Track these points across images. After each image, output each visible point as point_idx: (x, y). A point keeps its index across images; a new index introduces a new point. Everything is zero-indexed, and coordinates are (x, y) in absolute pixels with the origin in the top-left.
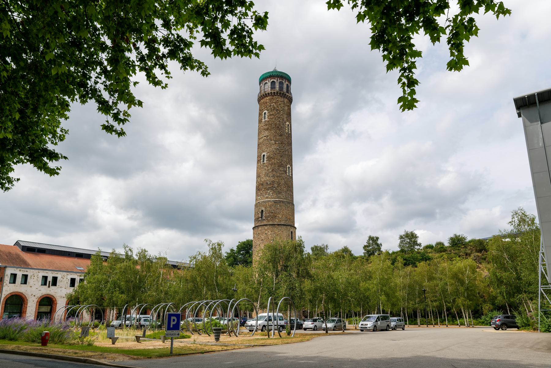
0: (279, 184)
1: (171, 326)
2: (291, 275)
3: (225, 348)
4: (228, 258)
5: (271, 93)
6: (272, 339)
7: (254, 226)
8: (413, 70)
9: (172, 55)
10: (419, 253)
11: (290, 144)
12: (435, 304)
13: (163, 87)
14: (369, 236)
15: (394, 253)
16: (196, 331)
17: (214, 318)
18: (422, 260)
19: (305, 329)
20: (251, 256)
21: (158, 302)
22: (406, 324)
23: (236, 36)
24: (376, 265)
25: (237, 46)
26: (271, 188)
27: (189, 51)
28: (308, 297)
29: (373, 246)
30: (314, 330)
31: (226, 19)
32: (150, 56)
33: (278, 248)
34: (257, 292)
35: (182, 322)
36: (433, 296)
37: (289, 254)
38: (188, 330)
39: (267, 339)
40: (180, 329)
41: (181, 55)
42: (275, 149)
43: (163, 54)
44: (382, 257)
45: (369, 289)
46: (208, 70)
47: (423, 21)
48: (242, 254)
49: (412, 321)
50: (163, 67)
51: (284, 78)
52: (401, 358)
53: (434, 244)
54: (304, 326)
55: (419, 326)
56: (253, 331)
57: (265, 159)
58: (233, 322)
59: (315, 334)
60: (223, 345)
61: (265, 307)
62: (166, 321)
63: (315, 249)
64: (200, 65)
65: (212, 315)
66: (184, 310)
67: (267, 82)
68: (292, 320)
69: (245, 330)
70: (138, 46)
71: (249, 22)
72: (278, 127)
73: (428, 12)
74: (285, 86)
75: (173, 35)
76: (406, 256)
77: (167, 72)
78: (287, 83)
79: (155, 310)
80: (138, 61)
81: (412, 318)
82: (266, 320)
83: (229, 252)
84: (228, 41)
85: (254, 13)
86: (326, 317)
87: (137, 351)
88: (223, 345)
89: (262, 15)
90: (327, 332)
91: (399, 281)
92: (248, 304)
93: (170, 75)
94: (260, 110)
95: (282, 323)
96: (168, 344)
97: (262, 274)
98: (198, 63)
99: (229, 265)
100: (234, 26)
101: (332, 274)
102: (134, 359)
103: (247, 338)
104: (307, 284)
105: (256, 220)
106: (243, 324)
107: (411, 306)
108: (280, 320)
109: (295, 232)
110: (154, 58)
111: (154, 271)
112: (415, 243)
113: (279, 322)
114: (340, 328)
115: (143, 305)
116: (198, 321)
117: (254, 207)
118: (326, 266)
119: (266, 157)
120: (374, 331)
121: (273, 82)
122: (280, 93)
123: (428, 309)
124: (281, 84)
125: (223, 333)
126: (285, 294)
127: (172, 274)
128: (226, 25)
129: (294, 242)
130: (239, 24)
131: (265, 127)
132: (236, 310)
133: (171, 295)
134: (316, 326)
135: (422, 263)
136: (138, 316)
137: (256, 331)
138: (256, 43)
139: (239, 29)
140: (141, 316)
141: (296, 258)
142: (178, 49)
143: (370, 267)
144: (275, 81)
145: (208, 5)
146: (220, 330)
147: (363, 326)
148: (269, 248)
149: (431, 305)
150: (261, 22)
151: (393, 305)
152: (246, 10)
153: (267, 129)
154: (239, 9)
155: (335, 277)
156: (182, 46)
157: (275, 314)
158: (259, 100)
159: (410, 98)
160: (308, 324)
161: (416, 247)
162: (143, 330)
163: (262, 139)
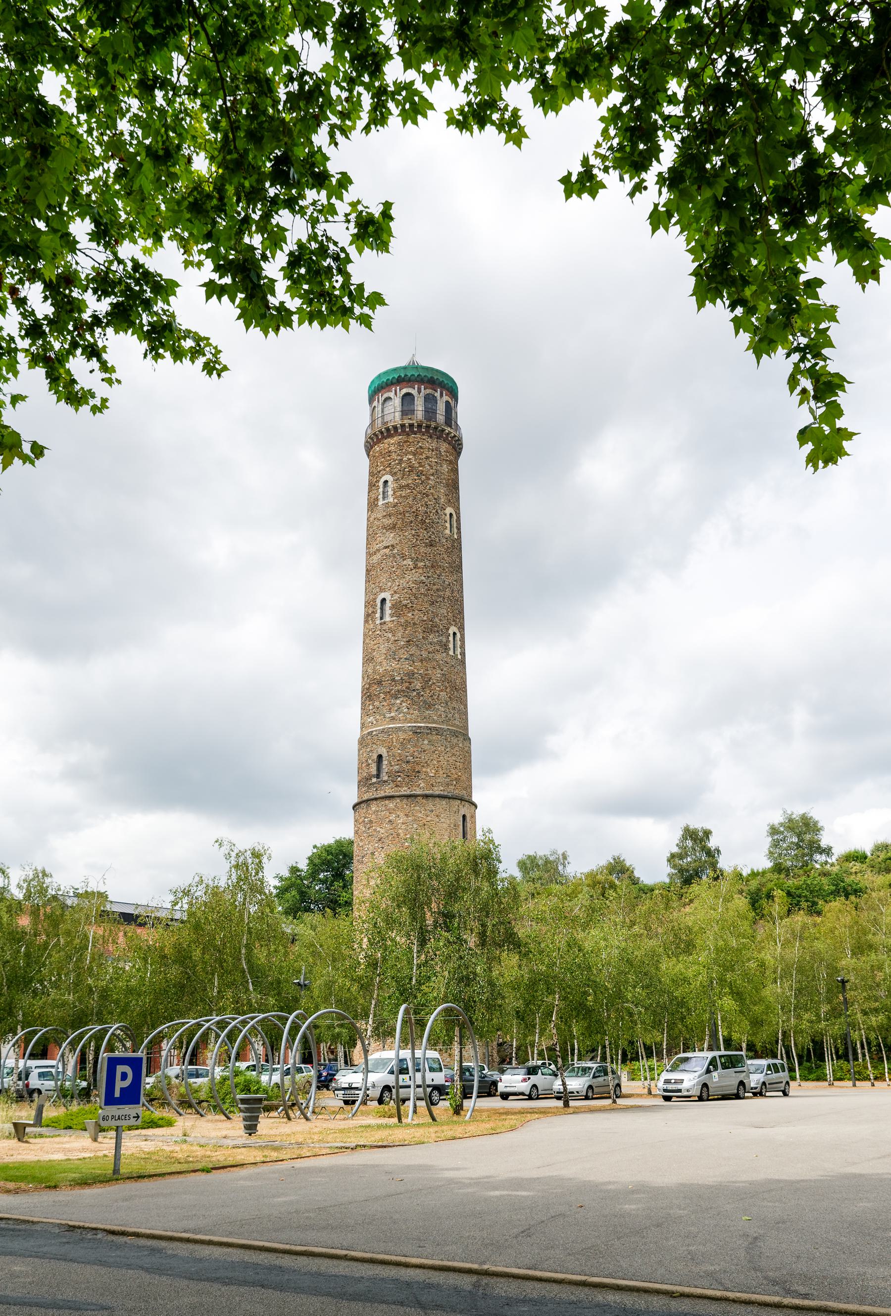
0: (427, 681)
1: (117, 1094)
2: (460, 941)
3: (274, 1155)
4: (282, 892)
5: (403, 426)
6: (408, 1125)
7: (356, 801)
8: (826, 352)
9: (121, 317)
10: (825, 874)
11: (457, 568)
12: (874, 1020)
13: (95, 409)
14: (683, 825)
15: (754, 874)
16: (190, 1106)
17: (243, 1065)
18: (836, 893)
19: (505, 1096)
20: (347, 885)
21: (79, 1020)
22: (793, 1079)
23: (303, 271)
24: (702, 909)
25: (308, 299)
26: (406, 693)
27: (166, 307)
28: (512, 1002)
29: (696, 860)
30: (530, 1098)
31: (274, 222)
32: (55, 322)
33: (426, 863)
34: (366, 987)
35: (150, 1080)
36: (868, 999)
37: (457, 880)
38: (165, 1103)
39: (395, 1126)
40: (143, 1099)
41: (145, 318)
42: (415, 582)
43: (95, 317)
44: (724, 886)
45: (686, 980)
46: (224, 359)
47: (829, 227)
48: (323, 882)
49: (810, 1071)
50: (93, 352)
51: (439, 384)
52: (779, 1181)
53: (867, 848)
54: (501, 1087)
55: (831, 1085)
56: (354, 1102)
57: (388, 611)
58: (298, 1077)
59: (532, 1111)
60: (266, 1147)
61: (391, 1033)
62: (103, 1076)
63: (528, 865)
64: (200, 347)
65: (238, 1058)
66: (155, 1044)
67: (392, 395)
68: (468, 1069)
69: (332, 1100)
70: (22, 295)
71: (340, 232)
72: (423, 522)
73: (841, 200)
74: (441, 408)
75: (120, 262)
76: (791, 883)
77: (105, 367)
78: (446, 398)
79: (73, 1045)
80: (22, 338)
81: (809, 1060)
82: (391, 1072)
83: (286, 874)
84: (282, 285)
85: (354, 205)
86: (564, 1059)
87: (18, 1168)
88: (266, 1147)
89: (376, 211)
90: (566, 1105)
91: (771, 955)
92: (342, 1026)
93: (114, 376)
94: (371, 474)
95: (439, 1078)
96: (107, 1143)
97: (379, 938)
98: (194, 339)
99: (287, 913)
100: (300, 245)
101: (580, 935)
102: (8, 1191)
103: (339, 1124)
104: (509, 967)
105: (364, 782)
106: (325, 1083)
107: (805, 1025)
108: (432, 1070)
109: (473, 816)
110: (71, 328)
111: (68, 933)
112: (816, 848)
113: (429, 1076)
114: (602, 1092)
115: (35, 1032)
116: (198, 1075)
117: (356, 746)
118: (560, 915)
119: (388, 604)
120: (701, 1099)
121: (408, 394)
122: (428, 427)
123: (855, 1035)
124: (430, 400)
125: (268, 1109)
126: (446, 996)
127: (121, 939)
128: (276, 238)
129: (470, 844)
130: (313, 237)
131: (387, 522)
132: (305, 1040)
133: (117, 1002)
134: (534, 1086)
135: (837, 904)
136: (21, 1063)
137: (364, 1103)
138: (361, 287)
139: (312, 252)
140: (32, 1063)
141: (478, 890)
142: (136, 301)
143: (690, 915)
144: (414, 392)
145: (223, 185)
146: (260, 1100)
147: (670, 1087)
148: (397, 863)
149: (866, 1024)
150: (373, 230)
151: (757, 1023)
152: (329, 197)
153: (393, 527)
154: (311, 195)
155: (588, 946)
156: (148, 294)
157: (418, 1053)
158: (369, 447)
159: (827, 429)
160: (512, 1080)
161: (817, 857)
162: (35, 1105)
163: (378, 556)
